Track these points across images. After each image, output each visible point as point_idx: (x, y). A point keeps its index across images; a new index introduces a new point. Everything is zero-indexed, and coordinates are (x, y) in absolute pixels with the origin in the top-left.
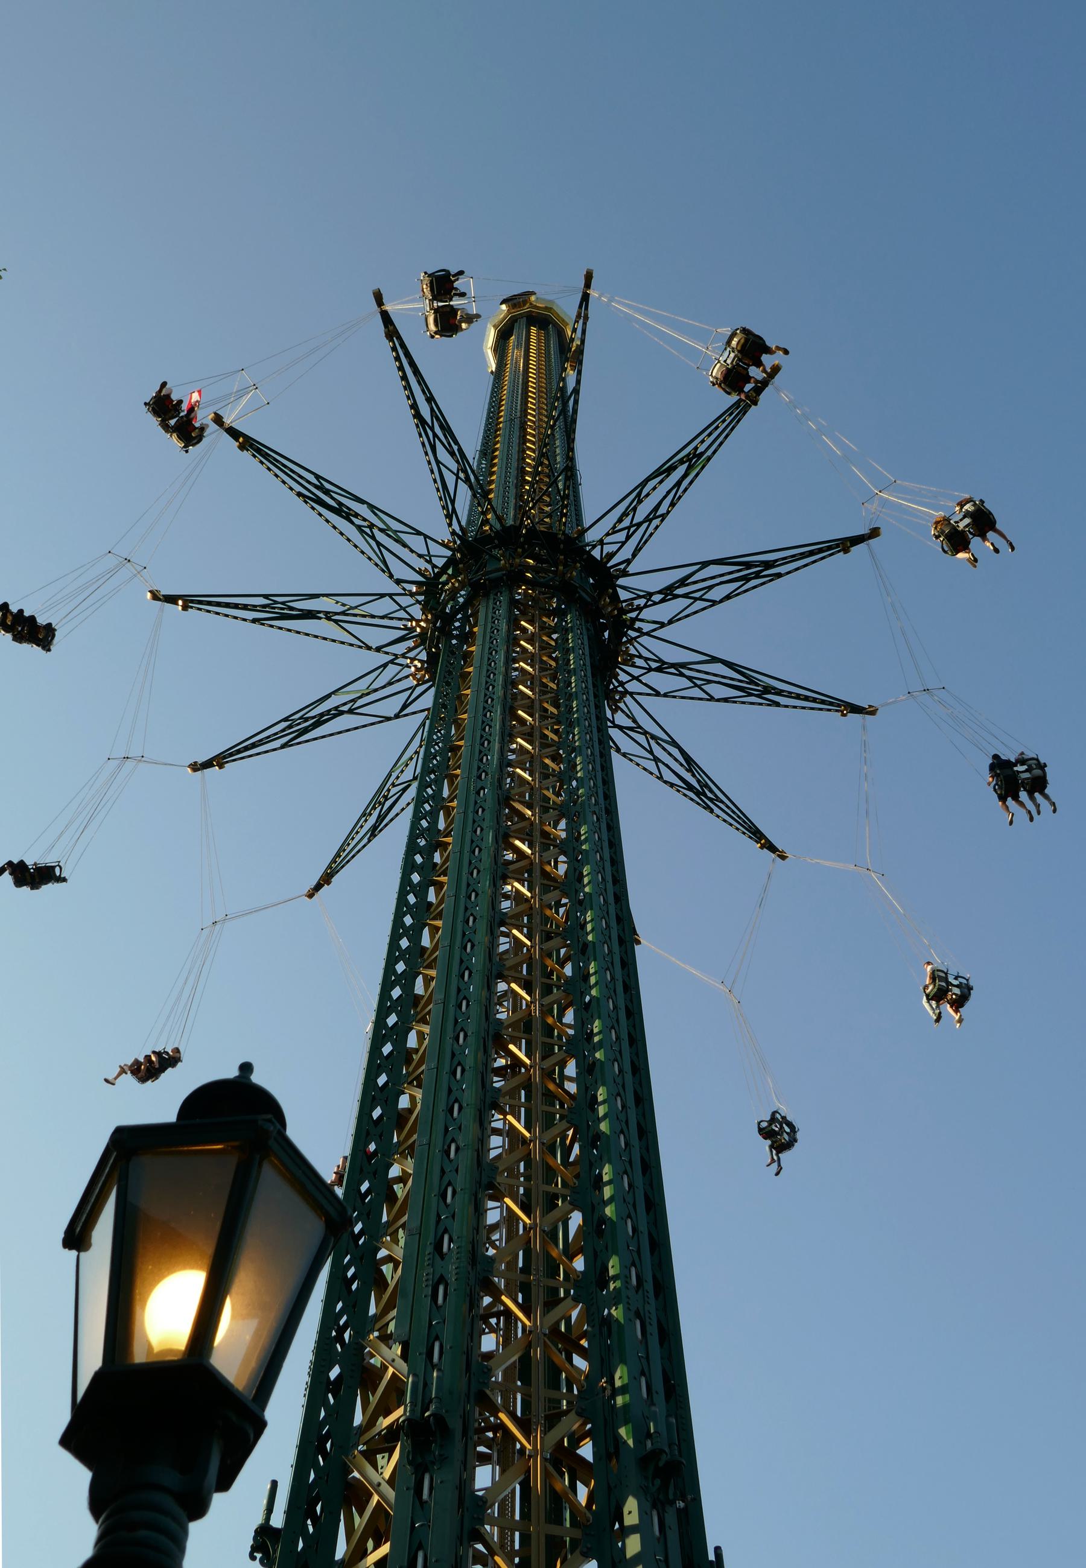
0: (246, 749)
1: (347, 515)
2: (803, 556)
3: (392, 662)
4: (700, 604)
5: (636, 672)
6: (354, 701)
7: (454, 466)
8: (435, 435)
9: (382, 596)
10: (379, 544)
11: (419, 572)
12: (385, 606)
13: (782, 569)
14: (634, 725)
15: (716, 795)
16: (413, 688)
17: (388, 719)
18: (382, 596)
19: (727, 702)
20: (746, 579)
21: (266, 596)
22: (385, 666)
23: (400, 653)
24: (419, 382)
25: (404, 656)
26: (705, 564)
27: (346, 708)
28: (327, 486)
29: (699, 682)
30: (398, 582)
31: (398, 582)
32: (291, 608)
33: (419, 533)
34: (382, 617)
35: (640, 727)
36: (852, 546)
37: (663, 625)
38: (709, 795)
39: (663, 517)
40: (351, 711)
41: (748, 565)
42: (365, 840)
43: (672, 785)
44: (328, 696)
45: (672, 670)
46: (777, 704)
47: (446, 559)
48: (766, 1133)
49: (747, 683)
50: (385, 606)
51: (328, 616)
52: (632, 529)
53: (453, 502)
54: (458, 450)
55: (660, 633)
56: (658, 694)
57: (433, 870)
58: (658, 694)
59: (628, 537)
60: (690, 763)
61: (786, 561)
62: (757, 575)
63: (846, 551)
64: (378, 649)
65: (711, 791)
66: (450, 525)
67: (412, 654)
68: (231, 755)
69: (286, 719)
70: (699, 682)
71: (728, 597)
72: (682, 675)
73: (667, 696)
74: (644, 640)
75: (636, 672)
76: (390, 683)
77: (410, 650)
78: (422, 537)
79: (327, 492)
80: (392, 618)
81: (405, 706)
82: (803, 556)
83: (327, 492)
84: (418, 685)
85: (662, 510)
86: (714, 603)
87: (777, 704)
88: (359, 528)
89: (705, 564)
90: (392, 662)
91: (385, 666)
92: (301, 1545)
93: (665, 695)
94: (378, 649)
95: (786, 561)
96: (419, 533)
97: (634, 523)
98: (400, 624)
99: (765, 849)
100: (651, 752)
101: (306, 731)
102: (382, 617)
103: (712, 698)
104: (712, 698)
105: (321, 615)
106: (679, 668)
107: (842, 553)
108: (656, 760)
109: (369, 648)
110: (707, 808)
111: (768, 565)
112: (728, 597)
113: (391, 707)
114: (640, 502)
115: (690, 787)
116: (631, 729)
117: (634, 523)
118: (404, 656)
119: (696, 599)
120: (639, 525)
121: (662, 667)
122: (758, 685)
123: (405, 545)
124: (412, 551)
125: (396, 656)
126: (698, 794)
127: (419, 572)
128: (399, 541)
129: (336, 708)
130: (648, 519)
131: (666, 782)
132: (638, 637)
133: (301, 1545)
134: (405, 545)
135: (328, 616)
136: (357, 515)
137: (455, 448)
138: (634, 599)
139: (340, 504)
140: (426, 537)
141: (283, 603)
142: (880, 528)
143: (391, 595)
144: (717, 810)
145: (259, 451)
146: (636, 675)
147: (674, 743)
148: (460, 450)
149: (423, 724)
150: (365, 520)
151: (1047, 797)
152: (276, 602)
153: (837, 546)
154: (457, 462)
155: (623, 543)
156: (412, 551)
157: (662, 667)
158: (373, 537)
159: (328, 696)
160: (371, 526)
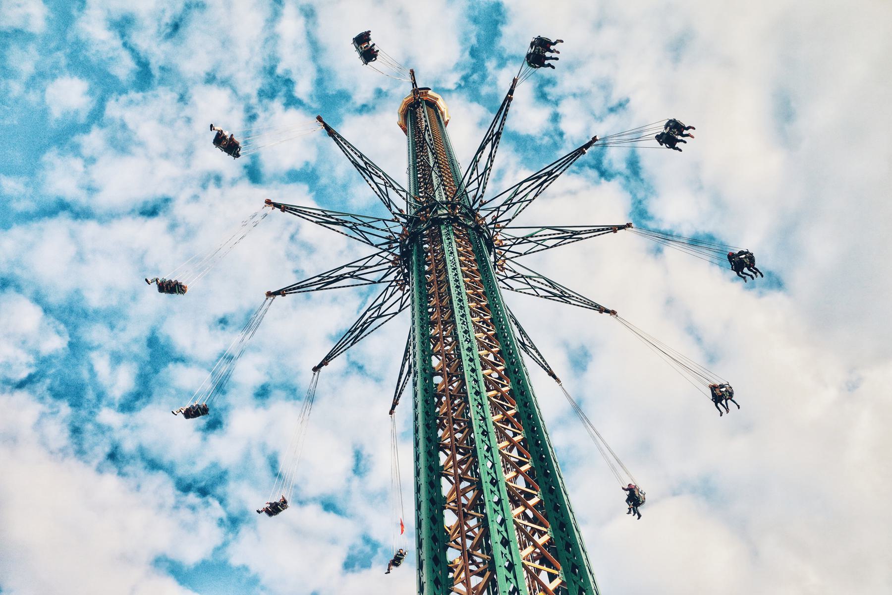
0: (298, 288)
1: (339, 278)
2: (594, 231)
3: (390, 286)
5: (506, 248)
7: (383, 182)
8: (370, 172)
9: (374, 256)
10: (361, 231)
11: (386, 238)
12: (377, 259)
13: (583, 236)
15: (569, 295)
16: (402, 297)
17: (396, 313)
18: (374, 256)
19: (556, 246)
20: (565, 238)
22: (387, 289)
27: (375, 315)
28: (329, 213)
32: (332, 277)
33: (379, 220)
35: (519, 274)
36: (618, 230)
37: (510, 220)
38: (566, 295)
40: (352, 277)
43: (545, 297)
44: (343, 267)
45: (522, 280)
46: (582, 239)
49: (563, 233)
50: (377, 259)
52: (511, 205)
53: (387, 196)
55: (510, 225)
56: (521, 255)
58: (521, 255)
60: (552, 284)
61: (586, 232)
62: (571, 237)
63: (615, 231)
65: (566, 293)
66: (391, 210)
67: (398, 278)
68: (290, 290)
70: (539, 242)
72: (530, 241)
73: (526, 254)
74: (503, 231)
75: (506, 248)
76: (378, 265)
77: (396, 277)
79: (329, 216)
80: (380, 264)
81: (401, 306)
82: (594, 231)
83: (329, 216)
85: (489, 166)
87: (582, 239)
88: (350, 228)
89: (521, 184)
90: (390, 286)
91: (387, 289)
93: (525, 254)
95: (586, 232)
96: (379, 220)
100: (528, 284)
101: (357, 336)
103: (548, 248)
104: (548, 248)
105: (347, 276)
106: (525, 239)
107: (613, 233)
108: (533, 287)
110: (567, 302)
115: (555, 295)
118: (394, 280)
122: (568, 233)
123: (373, 228)
124: (378, 229)
126: (560, 297)
127: (386, 238)
128: (370, 226)
129: (370, 317)
132: (500, 230)
134: (373, 228)
136: (346, 222)
137: (381, 174)
138: (504, 240)
139: (337, 219)
140: (384, 220)
141: (327, 276)
143: (377, 254)
144: (572, 302)
145: (291, 209)
147: (540, 276)
148: (383, 174)
150: (351, 222)
151: (688, 128)
153: (611, 229)
154: (383, 179)
156: (378, 229)
159: (343, 267)
160: (355, 224)
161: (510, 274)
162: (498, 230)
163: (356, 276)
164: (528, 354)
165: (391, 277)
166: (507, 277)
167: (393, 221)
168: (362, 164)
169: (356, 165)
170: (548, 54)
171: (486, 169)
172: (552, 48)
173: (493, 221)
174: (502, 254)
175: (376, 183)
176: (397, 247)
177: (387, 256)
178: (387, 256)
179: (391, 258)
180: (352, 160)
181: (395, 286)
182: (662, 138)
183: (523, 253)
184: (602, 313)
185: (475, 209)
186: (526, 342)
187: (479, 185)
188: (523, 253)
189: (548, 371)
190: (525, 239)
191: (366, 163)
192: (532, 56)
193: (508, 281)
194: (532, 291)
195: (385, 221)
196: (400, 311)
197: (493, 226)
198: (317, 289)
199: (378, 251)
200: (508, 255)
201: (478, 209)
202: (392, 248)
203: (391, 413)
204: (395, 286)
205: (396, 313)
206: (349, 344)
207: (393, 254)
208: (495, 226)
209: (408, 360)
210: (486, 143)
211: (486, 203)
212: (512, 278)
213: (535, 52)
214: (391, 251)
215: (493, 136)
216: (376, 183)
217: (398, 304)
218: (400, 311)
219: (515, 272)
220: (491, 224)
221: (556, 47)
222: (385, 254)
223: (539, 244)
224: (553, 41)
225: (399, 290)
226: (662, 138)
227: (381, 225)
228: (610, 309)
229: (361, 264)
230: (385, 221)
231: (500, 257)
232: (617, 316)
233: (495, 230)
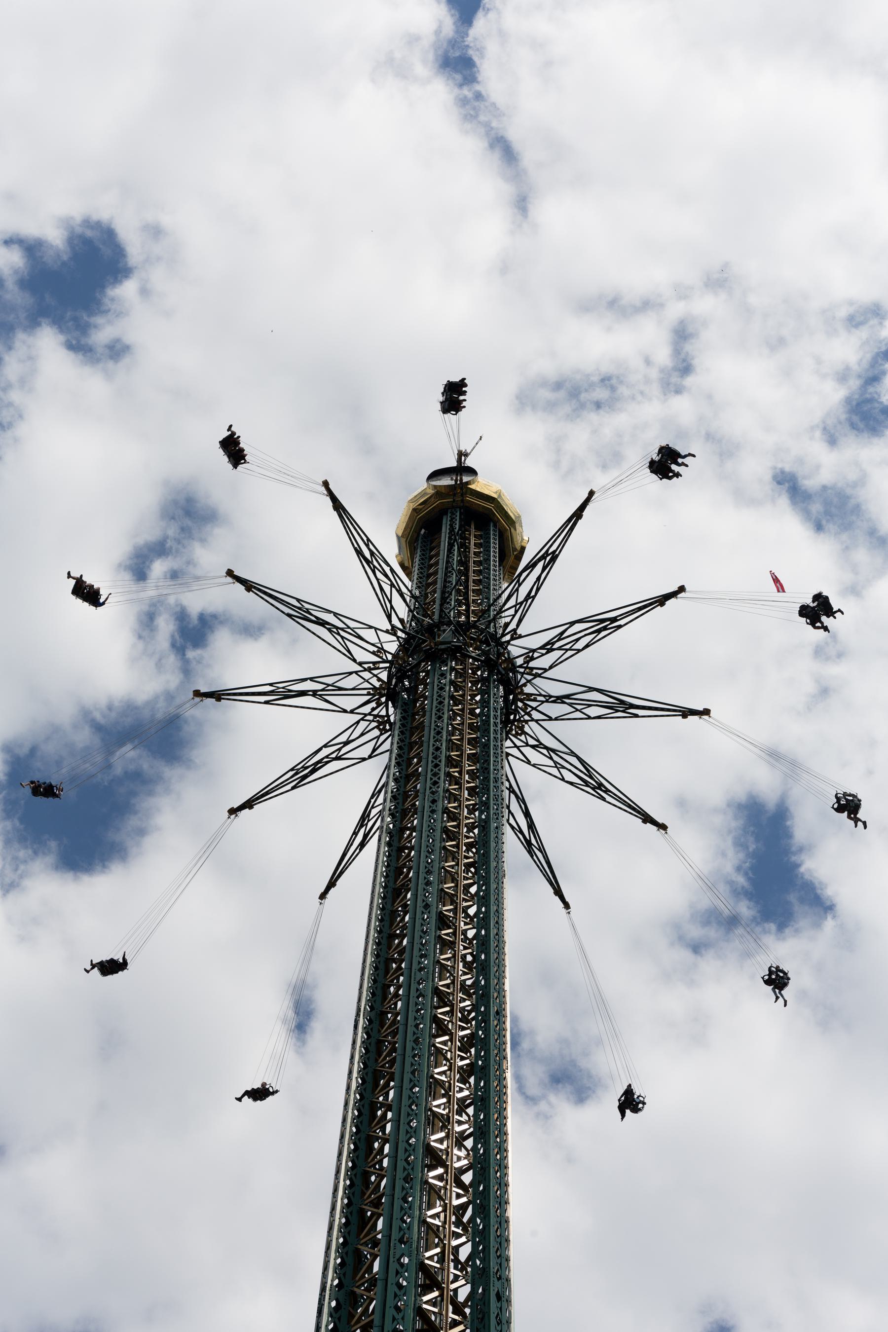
1: (321, 764)
2: (640, 609)
3: (362, 719)
4: (570, 653)
6: (340, 749)
9: (351, 673)
10: (342, 638)
12: (353, 681)
14: (538, 743)
16: (378, 737)
17: (364, 759)
18: (351, 673)
20: (599, 631)
21: (271, 685)
22: (358, 722)
23: (367, 712)
24: (352, 845)
25: (370, 714)
26: (572, 624)
27: (334, 756)
29: (579, 707)
30: (360, 664)
31: (360, 664)
32: (290, 691)
34: (353, 689)
35: (541, 744)
39: (534, 597)
40: (338, 758)
41: (602, 621)
42: (358, 851)
45: (545, 751)
47: (385, 708)
48: (840, 809)
50: (353, 681)
51: (315, 693)
52: (518, 607)
53: (390, 602)
54: (372, 799)
56: (550, 719)
57: (353, 1279)
59: (516, 612)
62: (605, 628)
64: (352, 712)
67: (375, 712)
69: (292, 769)
70: (579, 707)
71: (587, 646)
72: (551, 758)
74: (537, 681)
75: (534, 704)
76: (362, 734)
77: (373, 709)
78: (373, 629)
81: (374, 750)
82: (640, 609)
84: (381, 734)
85: (533, 594)
86: (579, 651)
87: (636, 716)
89: (572, 624)
90: (362, 719)
91: (358, 722)
92: (461, 1212)
94: (352, 712)
97: (518, 602)
98: (365, 692)
99: (689, 717)
101: (306, 777)
102: (353, 689)
104: (589, 718)
109: (345, 711)
111: (614, 620)
112: (587, 646)
113: (365, 751)
114: (520, 585)
115: (587, 784)
116: (537, 746)
117: (518, 602)
118: (370, 714)
119: (567, 650)
120: (521, 603)
121: (538, 746)
125: (366, 715)
129: (327, 757)
130: (526, 599)
131: (567, 782)
133: (461, 1212)
135: (315, 693)
140: (376, 629)
142: (684, 586)
143: (356, 672)
146: (534, 706)
149: (388, 767)
152: (279, 688)
155: (514, 616)
157: (538, 746)
158: (339, 634)
161: (532, 742)
162: (529, 677)
163: (320, 695)
164: (532, 857)
165: (367, 709)
166: (527, 745)
167: (387, 632)
168: (367, 554)
169: (359, 552)
170: (674, 467)
171: (528, 596)
172: (680, 460)
173: (525, 663)
174: (528, 711)
175: (378, 580)
176: (386, 668)
177: (369, 679)
178: (369, 679)
179: (374, 681)
180: (356, 546)
181: (371, 721)
182: (804, 611)
183: (553, 718)
184: (646, 823)
185: (505, 642)
186: (533, 841)
187: (516, 612)
188: (553, 718)
189: (554, 888)
190: (560, 699)
191: (372, 554)
192: (656, 464)
193: (527, 751)
194: (554, 771)
195: (378, 631)
196: (370, 757)
197: (522, 670)
198: (267, 702)
199: (360, 669)
200: (536, 715)
201: (508, 642)
202: (378, 668)
203: (323, 896)
204: (371, 721)
205: (364, 759)
206: (289, 787)
207: (379, 680)
208: (525, 671)
209: (365, 827)
210: (539, 560)
211: (520, 637)
212: (533, 747)
213: (661, 461)
214: (375, 672)
215: (548, 555)
216: (378, 580)
217: (371, 745)
218: (370, 757)
219: (538, 740)
220: (521, 666)
221: (686, 461)
222: (366, 675)
223: (577, 710)
224: (683, 454)
225: (376, 729)
226: (804, 611)
227: (369, 635)
228: (660, 821)
229: (343, 738)
230: (378, 631)
231: (523, 713)
232: (666, 833)
233: (525, 675)
